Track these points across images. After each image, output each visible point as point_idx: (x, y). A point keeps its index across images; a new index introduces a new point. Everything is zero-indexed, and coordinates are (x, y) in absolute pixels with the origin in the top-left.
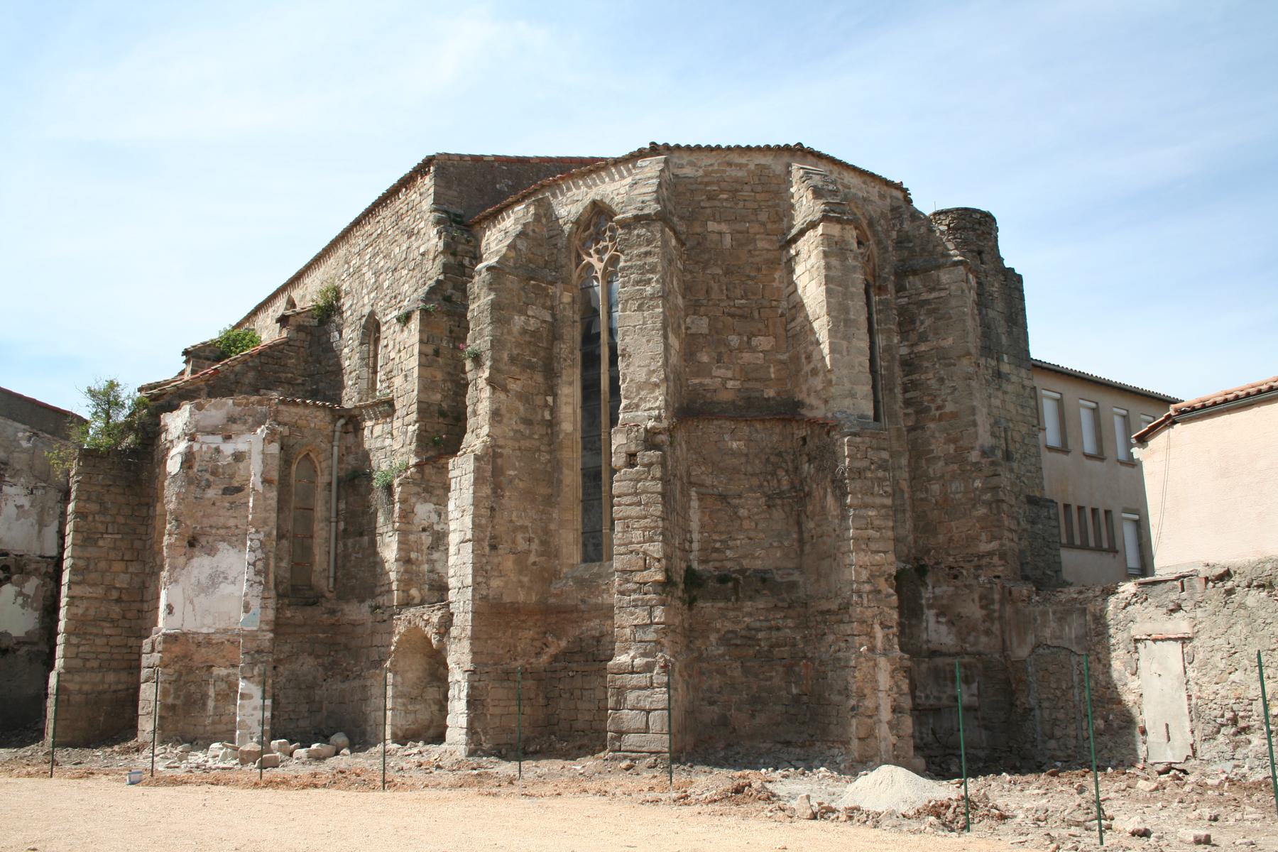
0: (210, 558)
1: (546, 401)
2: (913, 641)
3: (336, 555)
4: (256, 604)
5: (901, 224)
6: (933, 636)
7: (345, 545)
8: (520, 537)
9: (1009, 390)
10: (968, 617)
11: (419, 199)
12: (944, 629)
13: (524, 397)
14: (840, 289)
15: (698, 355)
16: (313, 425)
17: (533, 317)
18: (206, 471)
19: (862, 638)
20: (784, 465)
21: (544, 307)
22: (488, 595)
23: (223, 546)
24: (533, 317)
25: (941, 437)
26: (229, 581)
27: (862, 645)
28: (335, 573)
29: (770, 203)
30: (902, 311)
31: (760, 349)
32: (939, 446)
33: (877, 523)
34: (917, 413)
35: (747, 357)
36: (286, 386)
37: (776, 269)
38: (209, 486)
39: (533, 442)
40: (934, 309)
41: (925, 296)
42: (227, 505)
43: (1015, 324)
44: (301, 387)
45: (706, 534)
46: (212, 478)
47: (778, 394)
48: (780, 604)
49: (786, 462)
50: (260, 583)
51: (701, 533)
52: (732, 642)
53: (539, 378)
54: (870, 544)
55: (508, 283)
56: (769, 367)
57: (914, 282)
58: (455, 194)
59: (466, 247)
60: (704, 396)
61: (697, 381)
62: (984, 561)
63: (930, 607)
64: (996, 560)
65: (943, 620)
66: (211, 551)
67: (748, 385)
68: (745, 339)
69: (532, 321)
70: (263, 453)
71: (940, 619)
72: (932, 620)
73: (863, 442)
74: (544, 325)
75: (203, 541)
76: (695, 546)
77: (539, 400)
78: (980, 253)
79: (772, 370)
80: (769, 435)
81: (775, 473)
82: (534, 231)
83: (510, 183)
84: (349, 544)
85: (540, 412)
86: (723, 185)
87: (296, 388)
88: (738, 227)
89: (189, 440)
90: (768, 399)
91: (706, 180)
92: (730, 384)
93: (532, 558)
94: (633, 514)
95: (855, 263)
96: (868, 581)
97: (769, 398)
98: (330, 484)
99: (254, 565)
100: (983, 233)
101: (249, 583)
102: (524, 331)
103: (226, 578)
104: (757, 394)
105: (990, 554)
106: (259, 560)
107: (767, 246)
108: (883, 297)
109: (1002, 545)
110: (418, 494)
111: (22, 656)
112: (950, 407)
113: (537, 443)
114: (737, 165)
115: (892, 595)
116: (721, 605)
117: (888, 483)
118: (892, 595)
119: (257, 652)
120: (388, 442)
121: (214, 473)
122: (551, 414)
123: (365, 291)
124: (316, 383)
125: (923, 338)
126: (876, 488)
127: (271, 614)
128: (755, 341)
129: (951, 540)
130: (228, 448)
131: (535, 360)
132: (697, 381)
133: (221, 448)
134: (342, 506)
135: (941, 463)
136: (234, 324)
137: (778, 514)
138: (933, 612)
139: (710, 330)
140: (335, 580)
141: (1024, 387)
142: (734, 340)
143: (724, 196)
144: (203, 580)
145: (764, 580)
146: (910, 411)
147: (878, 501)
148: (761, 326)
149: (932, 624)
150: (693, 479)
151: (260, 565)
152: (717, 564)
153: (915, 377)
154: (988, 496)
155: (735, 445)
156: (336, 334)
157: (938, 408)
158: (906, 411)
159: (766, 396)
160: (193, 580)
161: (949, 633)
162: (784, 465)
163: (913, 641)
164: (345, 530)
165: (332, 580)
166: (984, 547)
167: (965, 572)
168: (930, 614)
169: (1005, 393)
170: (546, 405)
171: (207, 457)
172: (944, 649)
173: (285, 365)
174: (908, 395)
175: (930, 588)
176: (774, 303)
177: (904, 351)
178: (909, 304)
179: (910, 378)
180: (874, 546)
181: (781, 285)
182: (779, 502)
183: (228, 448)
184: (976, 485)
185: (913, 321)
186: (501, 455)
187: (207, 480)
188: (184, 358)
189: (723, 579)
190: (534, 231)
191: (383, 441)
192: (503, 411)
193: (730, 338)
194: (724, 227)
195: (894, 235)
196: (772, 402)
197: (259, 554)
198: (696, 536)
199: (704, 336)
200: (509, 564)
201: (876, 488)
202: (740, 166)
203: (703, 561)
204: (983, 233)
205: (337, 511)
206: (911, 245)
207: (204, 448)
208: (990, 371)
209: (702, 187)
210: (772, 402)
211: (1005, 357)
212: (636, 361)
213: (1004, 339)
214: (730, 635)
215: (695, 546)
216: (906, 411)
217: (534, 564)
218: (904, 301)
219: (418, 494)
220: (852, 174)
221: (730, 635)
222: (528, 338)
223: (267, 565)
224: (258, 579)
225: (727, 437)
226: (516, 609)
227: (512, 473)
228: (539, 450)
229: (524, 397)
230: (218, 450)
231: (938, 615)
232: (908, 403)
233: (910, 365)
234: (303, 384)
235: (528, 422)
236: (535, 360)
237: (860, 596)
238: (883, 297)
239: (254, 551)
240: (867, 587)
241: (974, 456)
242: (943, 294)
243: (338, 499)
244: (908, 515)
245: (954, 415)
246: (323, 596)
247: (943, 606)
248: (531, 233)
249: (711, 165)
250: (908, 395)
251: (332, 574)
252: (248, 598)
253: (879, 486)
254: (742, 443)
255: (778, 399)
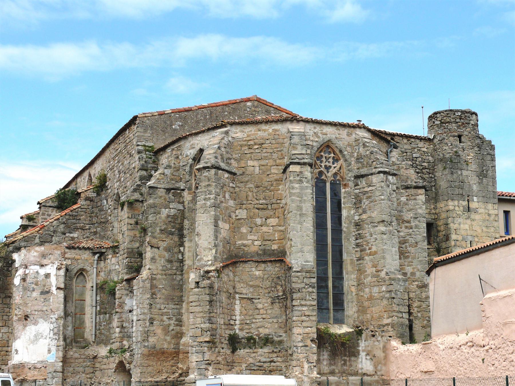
0: (35, 326)
1: (180, 250)
2: (351, 369)
3: (96, 323)
4: (54, 349)
5: (359, 149)
6: (364, 366)
7: (100, 318)
8: (165, 318)
9: (476, 218)
10: (378, 357)
11: (133, 137)
12: (368, 362)
13: (168, 249)
14: (298, 199)
15: (241, 229)
16: (83, 258)
17: (173, 208)
18: (33, 283)
19: (296, 368)
20: (280, 283)
21: (179, 203)
22: (148, 345)
23: (41, 320)
24: (173, 208)
25: (370, 264)
26: (44, 338)
27: (296, 371)
28: (96, 332)
29: (278, 149)
30: (357, 196)
31: (271, 225)
32: (370, 270)
33: (307, 314)
34: (361, 251)
35: (264, 229)
36: (80, 230)
37: (280, 184)
38: (34, 290)
39: (173, 271)
40: (369, 196)
41: (366, 189)
42: (42, 300)
43: (486, 176)
44: (88, 231)
45: (243, 317)
46: (35, 287)
47: (279, 247)
48: (275, 350)
49: (281, 281)
50: (56, 339)
51: (240, 315)
52: (252, 368)
53: (176, 239)
54: (303, 323)
55: (159, 193)
56: (275, 234)
57: (363, 182)
58: (149, 135)
59: (153, 165)
60: (244, 250)
61: (240, 242)
62: (385, 328)
63: (363, 351)
64: (390, 328)
65: (368, 357)
66: (36, 323)
67: (264, 243)
68: (264, 220)
69: (172, 210)
70: (56, 275)
71: (367, 358)
72: (364, 357)
73: (302, 275)
74: (179, 212)
75: (31, 317)
76: (237, 322)
77: (176, 250)
78: (460, 137)
79: (276, 235)
80: (273, 269)
81: (276, 287)
82: (174, 164)
83: (181, 124)
84: (101, 318)
85: (176, 255)
86: (256, 141)
87: (85, 231)
88: (263, 162)
89: (24, 268)
90: (274, 250)
91: (248, 139)
92: (256, 243)
93: (171, 328)
94: (197, 311)
95: (307, 185)
96: (302, 341)
97: (274, 250)
98: (92, 287)
99: (53, 330)
100: (463, 124)
101: (50, 339)
102: (168, 216)
103: (42, 336)
104: (269, 248)
105: (388, 325)
106: (55, 327)
107: (276, 172)
108: (347, 190)
109: (393, 320)
110: (127, 295)
111: (348, 325)
112: (374, 249)
113: (175, 271)
114: (263, 130)
115: (315, 347)
116: (248, 351)
117: (314, 294)
118: (315, 347)
119: (55, 372)
120: (117, 267)
121: (36, 284)
122: (182, 256)
123: (115, 181)
124: (96, 228)
125: (364, 212)
126: (308, 297)
127: (61, 354)
128: (269, 221)
129: (372, 317)
130: (42, 271)
131: (173, 230)
132: (240, 242)
133: (39, 272)
134: (98, 298)
135: (370, 278)
136: (62, 187)
137: (277, 306)
138: (365, 353)
139: (247, 217)
140: (96, 335)
141: (489, 215)
142: (259, 221)
143: (256, 147)
144: (32, 338)
145: (267, 341)
146: (358, 249)
147: (308, 303)
148: (272, 213)
149: (364, 360)
150: (237, 291)
151: (56, 330)
152: (248, 331)
153: (360, 232)
154: (387, 295)
155: (257, 273)
156: (105, 201)
157: (370, 249)
158: (356, 249)
159: (273, 249)
160: (27, 338)
161: (371, 365)
162: (280, 283)
163: (351, 369)
164: (100, 311)
165: (94, 336)
166: (386, 321)
167: (377, 333)
168: (363, 354)
169: (473, 220)
170: (180, 251)
171: (33, 276)
172: (368, 373)
173: (80, 219)
174: (358, 241)
175: (363, 341)
176: (278, 201)
177: (357, 218)
178: (359, 193)
179: (358, 232)
180: (304, 324)
181: (282, 192)
182: (277, 301)
183: (42, 271)
184: (383, 289)
185: (361, 203)
186: (155, 279)
187: (33, 288)
188: (39, 206)
189: (250, 339)
190: (174, 164)
191: (115, 266)
192: (157, 257)
193: (257, 220)
194: (256, 163)
195: (355, 154)
196: (275, 252)
197: (55, 325)
198: (238, 318)
199: (244, 219)
200: (159, 331)
201: (308, 297)
202: (265, 131)
203: (241, 330)
204: (463, 124)
205: (96, 301)
206: (362, 160)
207: (31, 271)
208: (462, 208)
209: (245, 143)
210: (275, 252)
211: (475, 199)
212: (203, 237)
213: (475, 187)
214: (252, 365)
215: (237, 322)
216: (356, 249)
217: (173, 330)
218: (357, 191)
219: (127, 295)
220: (329, 126)
221: (252, 365)
222: (170, 219)
223: (59, 330)
224: (55, 337)
225: (254, 269)
226: (163, 352)
227: (161, 287)
228: (175, 274)
229: (168, 249)
230: (37, 272)
231: (366, 355)
232: (357, 245)
233: (359, 226)
234: (89, 229)
235: (170, 261)
236: (173, 230)
237: (297, 348)
238: (347, 190)
239: (53, 324)
240: (301, 344)
241: (383, 274)
242: (373, 188)
243: (96, 295)
244: (354, 304)
245: (375, 253)
246: (90, 344)
247: (368, 351)
248: (173, 165)
249: (251, 131)
250: (358, 241)
251: (94, 333)
252: (50, 347)
253: (309, 296)
254: (261, 272)
255: (279, 250)
